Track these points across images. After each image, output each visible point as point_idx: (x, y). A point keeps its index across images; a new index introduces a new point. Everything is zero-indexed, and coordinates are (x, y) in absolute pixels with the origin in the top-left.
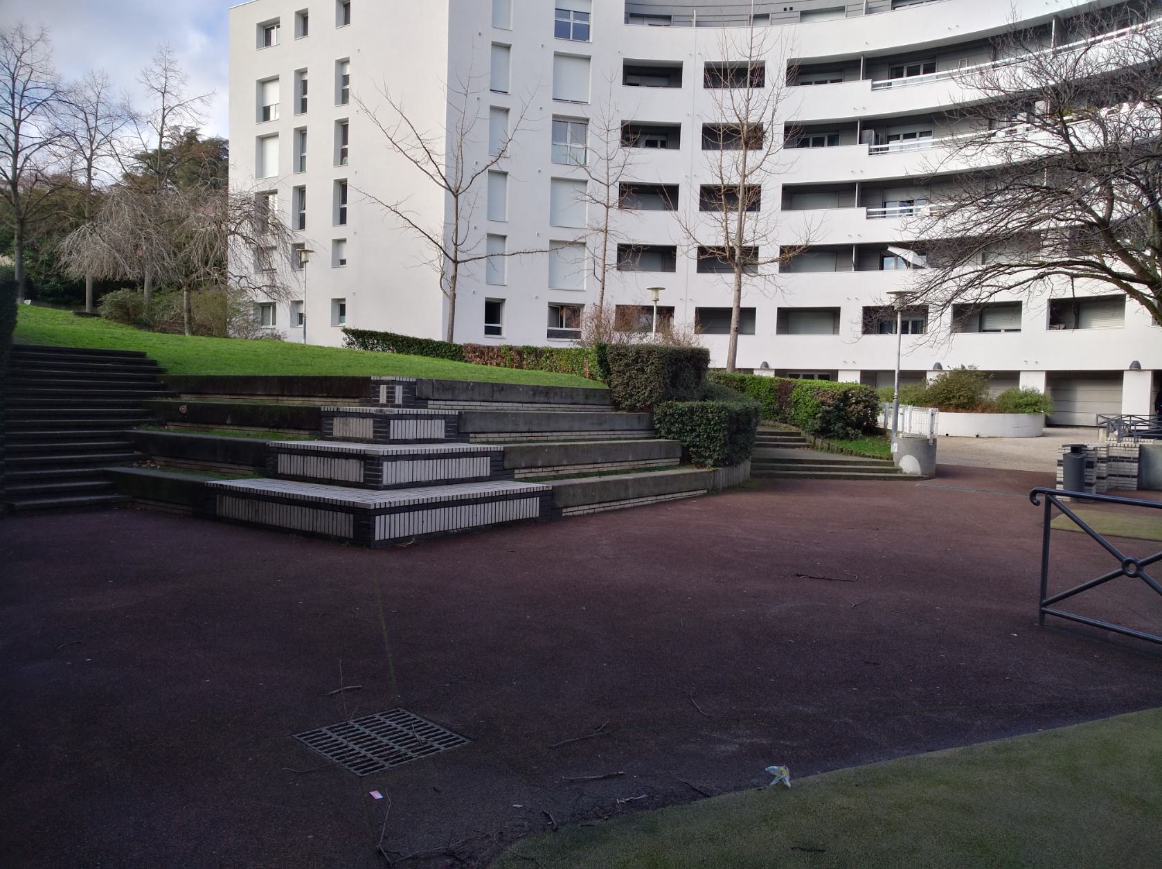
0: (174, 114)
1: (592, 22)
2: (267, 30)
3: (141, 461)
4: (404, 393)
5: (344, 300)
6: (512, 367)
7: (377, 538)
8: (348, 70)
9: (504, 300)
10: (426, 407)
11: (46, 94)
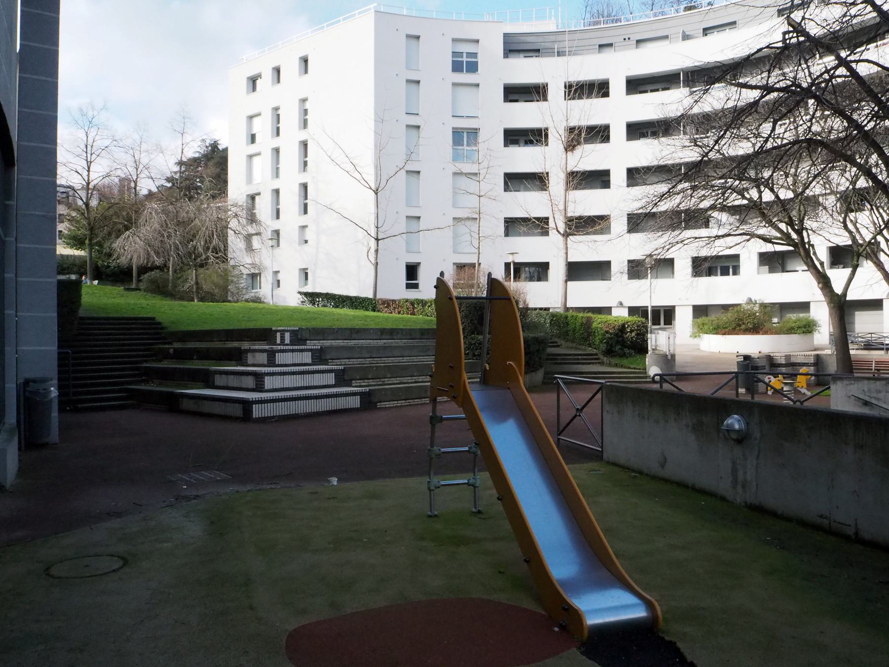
0: (189, 147)
1: (480, 60)
2: (253, 81)
3: (146, 382)
4: (290, 336)
5: (307, 269)
6: (408, 314)
7: (254, 417)
8: (308, 105)
9: (420, 263)
10: (305, 345)
11: (107, 142)
